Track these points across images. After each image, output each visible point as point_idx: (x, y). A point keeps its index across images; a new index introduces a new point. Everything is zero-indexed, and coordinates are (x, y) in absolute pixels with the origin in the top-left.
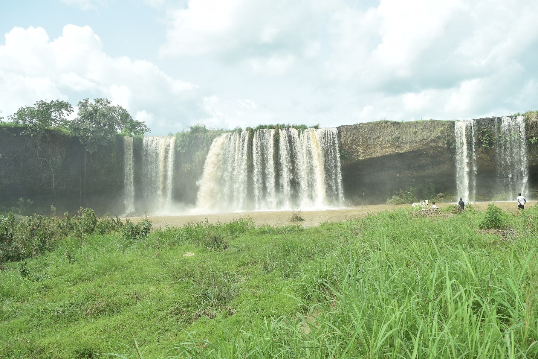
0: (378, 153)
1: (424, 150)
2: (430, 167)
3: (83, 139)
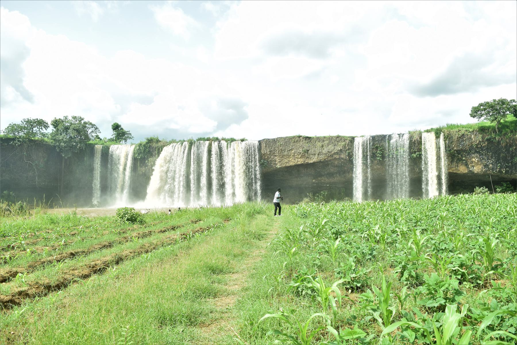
0: (292, 162)
1: (330, 160)
2: (338, 175)
3: (59, 147)
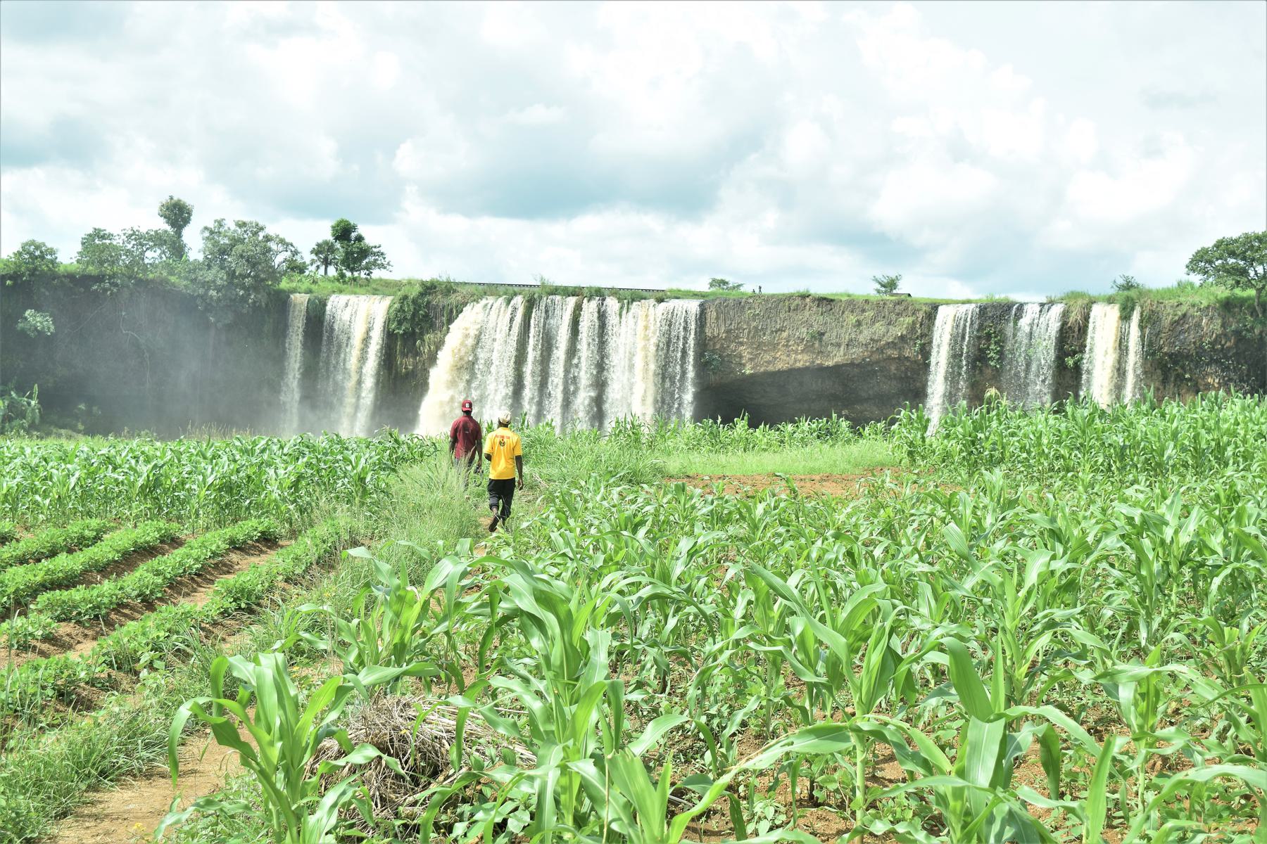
1: (877, 362)
